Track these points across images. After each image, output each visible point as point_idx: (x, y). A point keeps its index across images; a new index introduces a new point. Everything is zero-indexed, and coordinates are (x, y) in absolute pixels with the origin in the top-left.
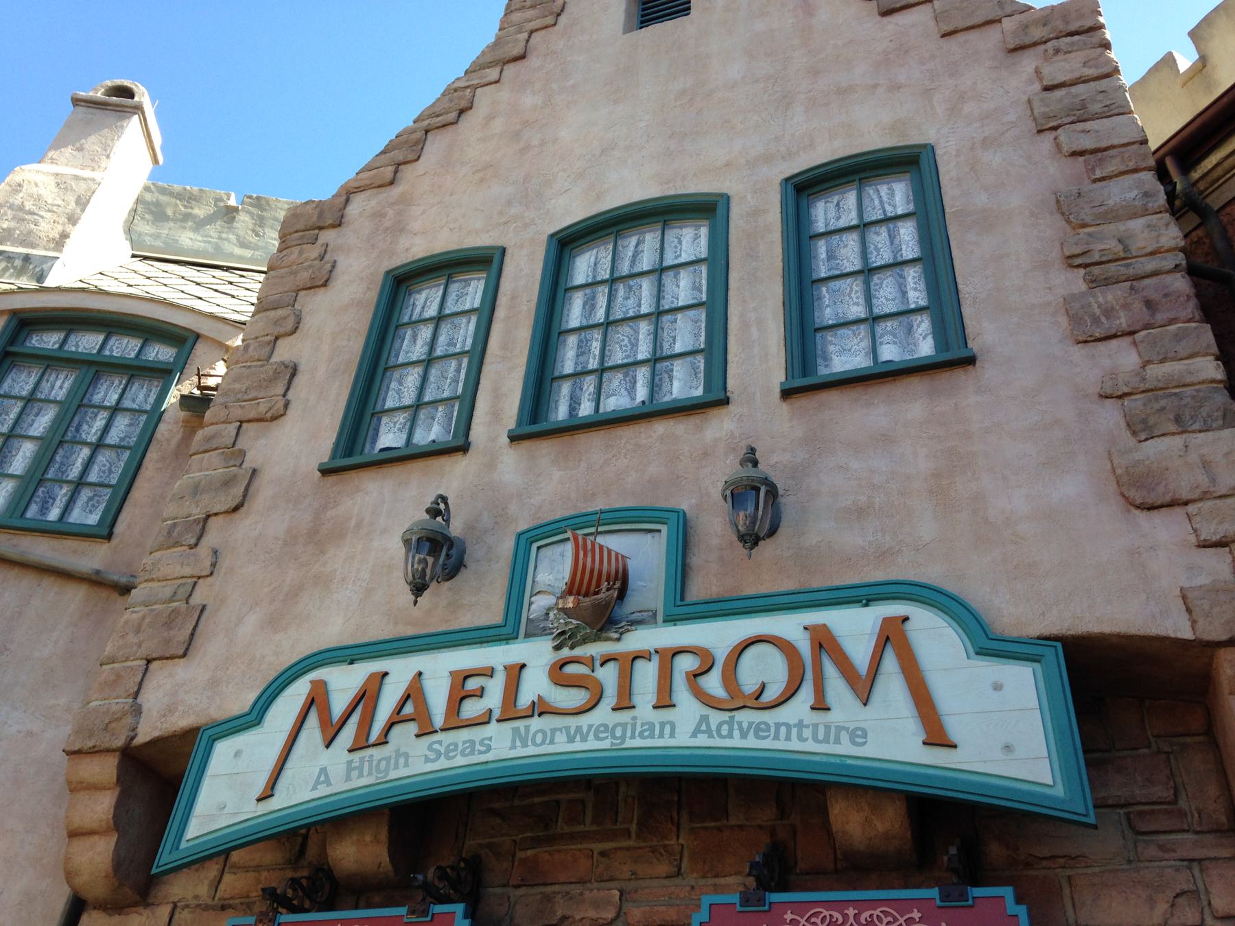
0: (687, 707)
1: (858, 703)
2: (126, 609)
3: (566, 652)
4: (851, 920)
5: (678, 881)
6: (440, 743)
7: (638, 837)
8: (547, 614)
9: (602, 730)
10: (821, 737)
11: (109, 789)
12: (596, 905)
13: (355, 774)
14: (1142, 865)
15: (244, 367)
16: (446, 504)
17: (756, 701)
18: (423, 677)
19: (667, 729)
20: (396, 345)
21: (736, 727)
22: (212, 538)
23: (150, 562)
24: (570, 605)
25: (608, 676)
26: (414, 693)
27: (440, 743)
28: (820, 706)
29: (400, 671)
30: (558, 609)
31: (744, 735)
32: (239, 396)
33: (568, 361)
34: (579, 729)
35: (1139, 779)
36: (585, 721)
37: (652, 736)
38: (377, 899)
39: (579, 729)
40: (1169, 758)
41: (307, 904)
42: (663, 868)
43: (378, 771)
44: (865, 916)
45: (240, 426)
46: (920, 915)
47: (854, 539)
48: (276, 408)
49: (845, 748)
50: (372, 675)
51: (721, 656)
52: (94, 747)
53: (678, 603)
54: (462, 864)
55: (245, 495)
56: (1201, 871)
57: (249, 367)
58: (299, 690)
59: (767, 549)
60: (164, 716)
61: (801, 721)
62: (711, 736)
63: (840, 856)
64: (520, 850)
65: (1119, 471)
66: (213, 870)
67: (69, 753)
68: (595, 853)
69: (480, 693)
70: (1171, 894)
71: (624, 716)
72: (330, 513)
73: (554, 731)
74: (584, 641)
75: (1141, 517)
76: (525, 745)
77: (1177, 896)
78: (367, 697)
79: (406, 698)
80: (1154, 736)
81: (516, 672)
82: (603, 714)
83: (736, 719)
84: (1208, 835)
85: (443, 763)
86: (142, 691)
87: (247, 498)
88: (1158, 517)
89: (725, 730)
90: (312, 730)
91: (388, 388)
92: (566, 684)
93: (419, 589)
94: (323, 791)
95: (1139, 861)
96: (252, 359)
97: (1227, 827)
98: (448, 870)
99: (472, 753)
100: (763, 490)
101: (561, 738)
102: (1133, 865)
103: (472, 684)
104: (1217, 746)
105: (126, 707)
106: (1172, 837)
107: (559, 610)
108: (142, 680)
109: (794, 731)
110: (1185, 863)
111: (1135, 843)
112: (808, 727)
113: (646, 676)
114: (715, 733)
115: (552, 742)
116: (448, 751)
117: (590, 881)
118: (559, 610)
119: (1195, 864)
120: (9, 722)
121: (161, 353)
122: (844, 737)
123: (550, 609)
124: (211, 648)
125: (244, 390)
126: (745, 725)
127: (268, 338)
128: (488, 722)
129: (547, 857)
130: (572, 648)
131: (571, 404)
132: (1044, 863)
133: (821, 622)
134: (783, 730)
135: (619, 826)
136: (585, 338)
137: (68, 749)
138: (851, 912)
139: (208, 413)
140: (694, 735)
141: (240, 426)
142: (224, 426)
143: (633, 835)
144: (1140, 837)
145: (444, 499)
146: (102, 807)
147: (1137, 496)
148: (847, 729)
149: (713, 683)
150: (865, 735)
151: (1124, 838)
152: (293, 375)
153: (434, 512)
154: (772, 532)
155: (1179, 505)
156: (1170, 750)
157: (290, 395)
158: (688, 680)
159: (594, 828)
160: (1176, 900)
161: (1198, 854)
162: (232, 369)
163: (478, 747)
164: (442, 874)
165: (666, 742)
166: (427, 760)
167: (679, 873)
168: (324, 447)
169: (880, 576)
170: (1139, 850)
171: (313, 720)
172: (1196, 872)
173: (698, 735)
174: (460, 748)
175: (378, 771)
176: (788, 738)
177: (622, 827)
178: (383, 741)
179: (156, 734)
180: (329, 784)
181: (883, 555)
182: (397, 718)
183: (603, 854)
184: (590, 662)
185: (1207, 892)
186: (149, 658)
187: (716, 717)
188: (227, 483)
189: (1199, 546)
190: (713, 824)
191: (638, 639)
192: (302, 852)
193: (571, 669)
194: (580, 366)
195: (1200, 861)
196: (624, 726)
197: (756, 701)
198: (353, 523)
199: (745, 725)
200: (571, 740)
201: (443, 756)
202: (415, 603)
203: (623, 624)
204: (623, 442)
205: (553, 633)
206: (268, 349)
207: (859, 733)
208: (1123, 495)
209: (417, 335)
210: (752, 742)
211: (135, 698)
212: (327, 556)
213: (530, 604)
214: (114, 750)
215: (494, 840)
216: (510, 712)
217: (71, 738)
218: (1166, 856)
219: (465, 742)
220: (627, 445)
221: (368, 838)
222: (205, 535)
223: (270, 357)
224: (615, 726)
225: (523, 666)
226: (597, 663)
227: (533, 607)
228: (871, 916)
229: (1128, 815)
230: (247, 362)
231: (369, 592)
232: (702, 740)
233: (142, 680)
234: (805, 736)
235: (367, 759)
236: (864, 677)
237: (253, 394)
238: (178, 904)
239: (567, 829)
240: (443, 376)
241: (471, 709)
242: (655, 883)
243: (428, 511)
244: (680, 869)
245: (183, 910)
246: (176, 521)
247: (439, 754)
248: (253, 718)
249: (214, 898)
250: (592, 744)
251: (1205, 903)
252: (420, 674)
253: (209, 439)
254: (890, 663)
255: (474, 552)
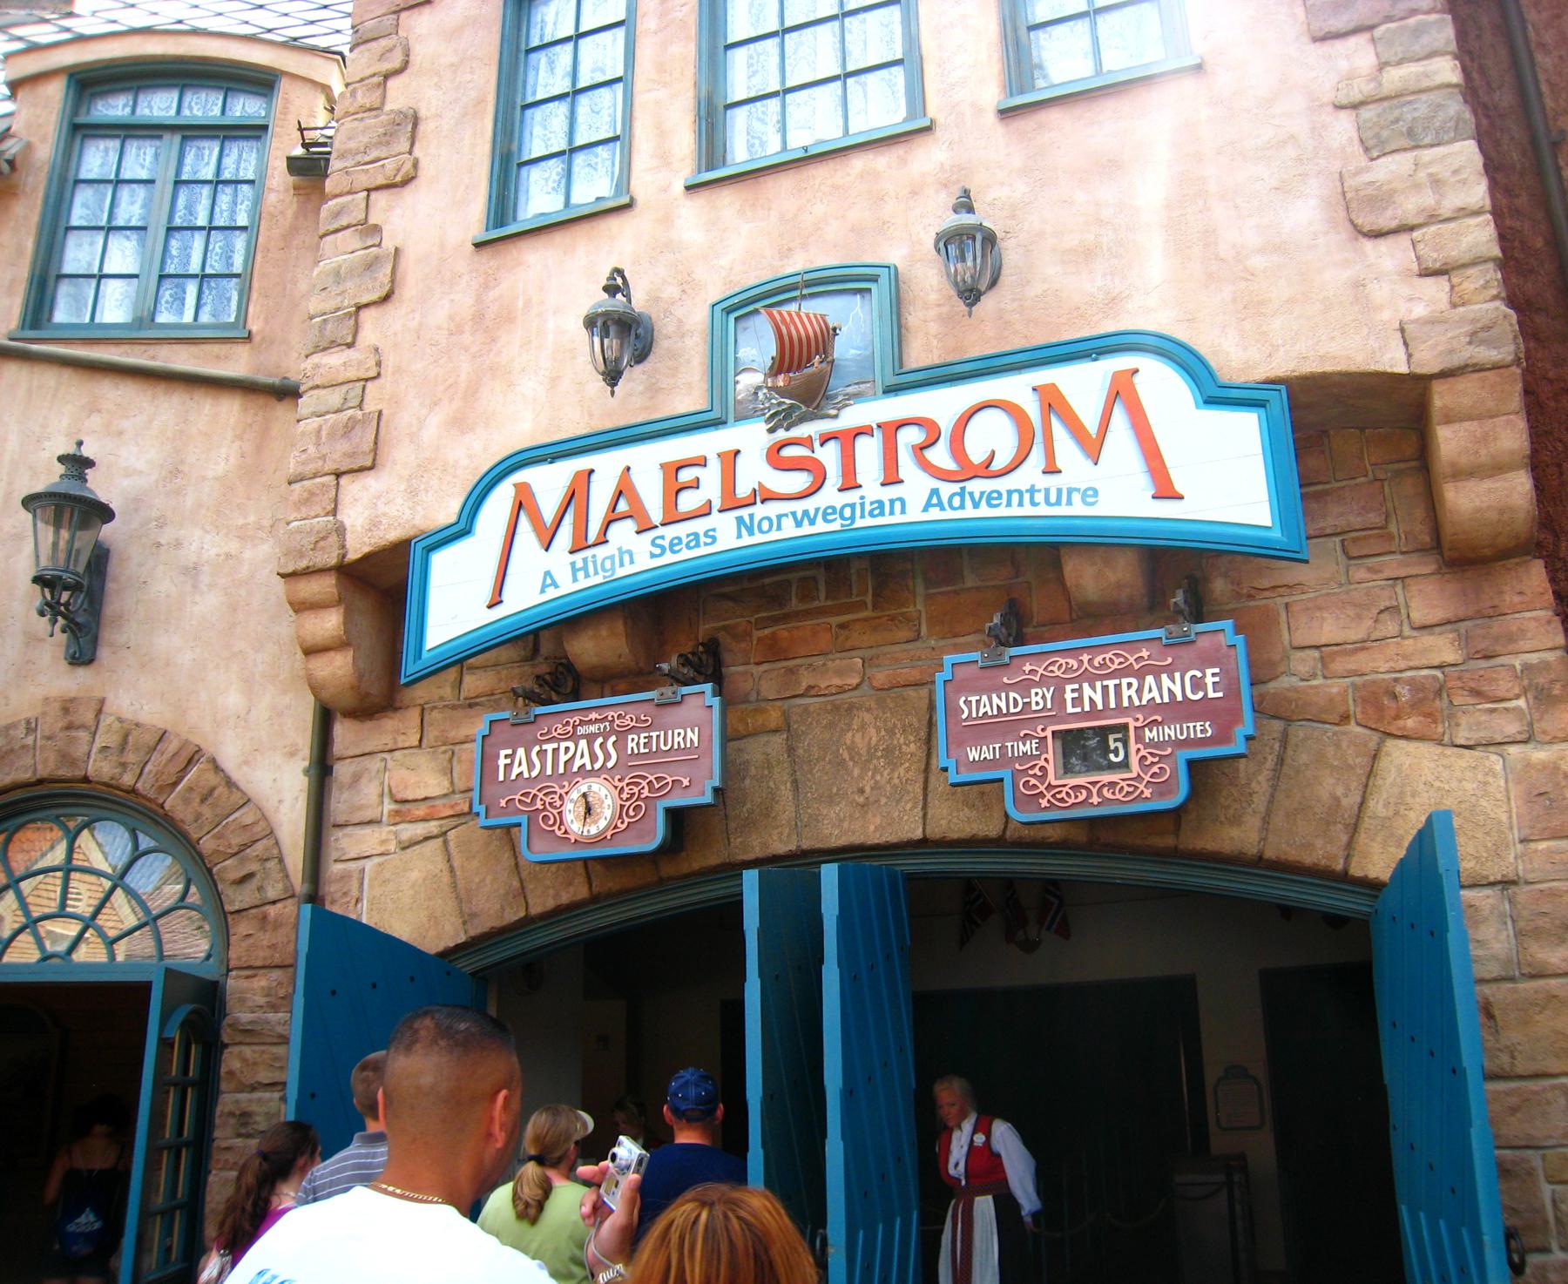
0: (916, 483)
1: (1089, 463)
2: (298, 421)
3: (781, 434)
4: (1086, 664)
5: (918, 644)
6: (662, 537)
7: (875, 607)
8: (756, 394)
9: (828, 513)
10: (1053, 499)
11: (333, 607)
12: (840, 673)
13: (581, 575)
14: (1352, 587)
15: (356, 119)
16: (624, 278)
17: (985, 470)
18: (631, 472)
19: (898, 505)
20: (531, 80)
21: (967, 497)
22: (370, 333)
23: (309, 367)
24: (781, 384)
25: (829, 455)
26: (624, 489)
27: (662, 537)
28: (1051, 470)
29: (606, 467)
30: (767, 387)
31: (976, 505)
32: (359, 158)
33: (739, 83)
34: (806, 513)
35: (1355, 508)
36: (810, 504)
37: (882, 514)
38: (622, 686)
39: (806, 513)
40: (1383, 486)
41: (555, 697)
42: (904, 634)
43: (604, 570)
44: (1098, 660)
45: (368, 196)
46: (1148, 653)
47: (1084, 286)
48: (404, 170)
49: (1077, 508)
50: (578, 475)
51: (946, 426)
52: (308, 567)
53: (897, 371)
54: (701, 648)
55: (393, 281)
56: (1404, 587)
57: (362, 119)
58: (501, 499)
59: (988, 303)
60: (370, 530)
61: (1033, 486)
62: (943, 509)
63: (1075, 607)
64: (757, 629)
65: (1349, 196)
66: (452, 673)
67: (283, 576)
68: (834, 627)
69: (695, 484)
70: (1375, 611)
71: (852, 496)
72: (493, 294)
73: (779, 517)
74: (802, 420)
75: (1368, 245)
76: (751, 533)
77: (1381, 612)
78: (577, 495)
79: (619, 494)
80: (1371, 465)
81: (730, 459)
82: (830, 495)
83: (967, 490)
84: (1412, 555)
85: (668, 558)
86: (340, 507)
87: (397, 283)
88: (1383, 245)
89: (956, 501)
90: (526, 532)
91: (531, 134)
92: (787, 467)
93: (612, 376)
94: (551, 593)
95: (1350, 583)
96: (364, 109)
97: (1429, 546)
98: (690, 656)
99: (697, 545)
100: (979, 237)
101: (788, 523)
102: (1344, 589)
103: (686, 475)
104: (1428, 471)
105: (329, 526)
106: (1381, 559)
107: (770, 389)
108: (336, 495)
109: (1027, 496)
110: (1390, 582)
111: (1348, 567)
112: (1039, 491)
113: (868, 452)
114: (946, 505)
115: (779, 528)
116: (672, 545)
117: (831, 652)
118: (770, 389)
119: (1399, 582)
120: (206, 547)
121: (246, 108)
122: (1076, 497)
123: (759, 388)
124: (401, 457)
125: (362, 149)
126: (977, 496)
127: (376, 80)
128: (709, 514)
129: (786, 634)
130: (787, 429)
131: (748, 140)
132: (1267, 594)
133: (1049, 381)
134: (1015, 497)
135: (854, 599)
136: (755, 50)
137: (282, 571)
138: (1085, 658)
139: (328, 182)
140: (925, 509)
141: (368, 196)
142: (349, 198)
143: (870, 606)
144: (1352, 562)
145: (620, 272)
146: (329, 623)
147: (1367, 221)
148: (1078, 490)
149: (940, 455)
150: (1096, 493)
151: (1337, 564)
152: (415, 126)
153: (611, 290)
154: (994, 283)
155: (1404, 230)
156: (1385, 477)
157: (417, 152)
158: (914, 452)
159: (829, 603)
160: (1382, 615)
161: (1402, 573)
162: (343, 124)
163: (703, 539)
164: (685, 661)
165: (898, 518)
166: (653, 556)
167: (918, 638)
168: (473, 217)
169: (1109, 327)
170: (1350, 573)
171: (524, 523)
172: (1399, 589)
173: (930, 509)
174: (685, 541)
175: (604, 570)
176: (1021, 504)
177: (858, 599)
178: (602, 541)
179: (367, 549)
180: (557, 586)
181: (1113, 302)
182: (613, 516)
183: (842, 626)
184: (807, 442)
185: (1407, 606)
186: (338, 471)
187: (947, 489)
188: (370, 265)
189: (1421, 275)
190: (949, 588)
191: (851, 417)
192: (536, 650)
193: (788, 452)
194: (754, 89)
195: (1403, 579)
196: (853, 506)
197: (985, 470)
198: (520, 304)
199: (977, 496)
200: (799, 524)
201: (668, 550)
202: (613, 393)
203: (840, 398)
204: (817, 182)
205: (764, 414)
206: (379, 92)
207: (1090, 492)
208: (1351, 221)
209: (553, 62)
210: (984, 511)
211: (335, 515)
212: (499, 345)
213: (736, 383)
214: (329, 569)
215: (727, 623)
216: (731, 503)
217: (282, 561)
218: (1375, 577)
219: (688, 536)
220: (822, 187)
221: (604, 633)
222: (360, 330)
223: (383, 103)
224: (843, 508)
225: (737, 452)
226: (817, 444)
227: (739, 387)
228: (1104, 659)
229: (1343, 541)
230: (357, 113)
231: (555, 381)
232: (935, 514)
233: (336, 495)
234: (1037, 500)
235: (590, 559)
236: (1094, 436)
237: (374, 154)
238: (426, 706)
239: (802, 607)
240: (593, 111)
241: (688, 501)
242: (897, 648)
243: (606, 289)
244: (919, 634)
245: (432, 710)
246: (325, 317)
247: (663, 548)
248: (461, 530)
249: (459, 699)
250: (821, 526)
251: (1404, 616)
252: (628, 469)
253: (337, 214)
254: (1119, 417)
255: (665, 328)
